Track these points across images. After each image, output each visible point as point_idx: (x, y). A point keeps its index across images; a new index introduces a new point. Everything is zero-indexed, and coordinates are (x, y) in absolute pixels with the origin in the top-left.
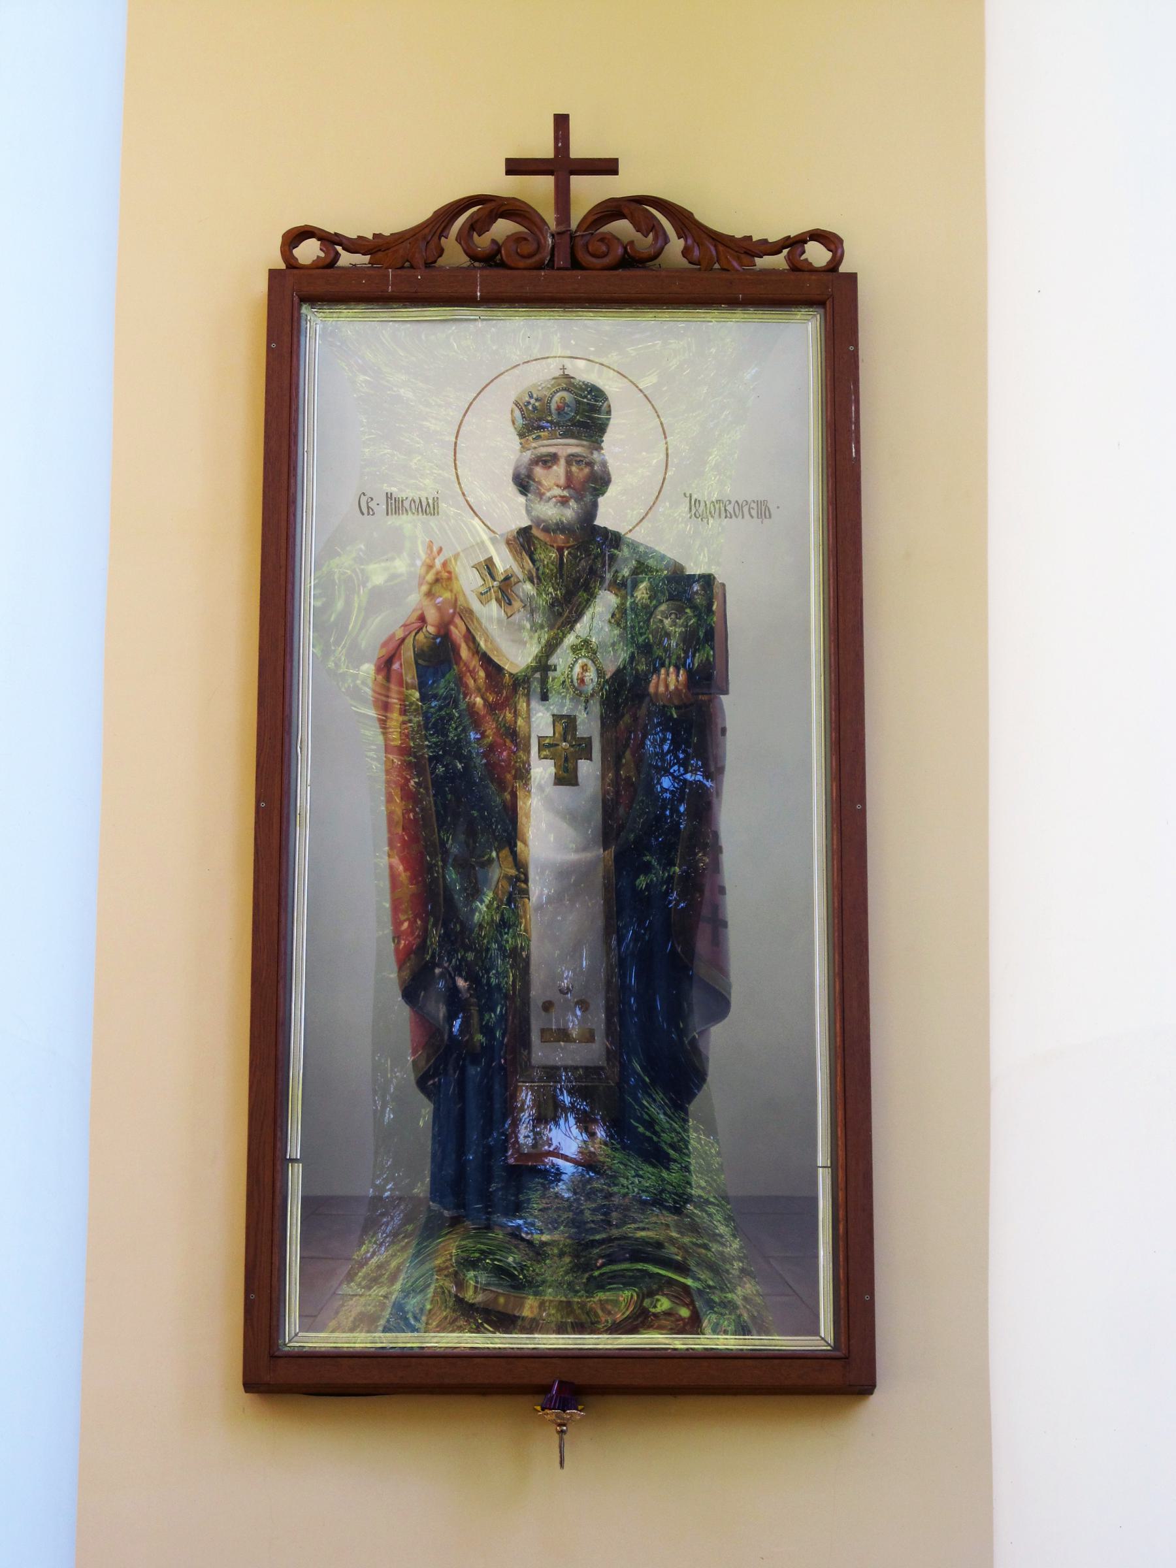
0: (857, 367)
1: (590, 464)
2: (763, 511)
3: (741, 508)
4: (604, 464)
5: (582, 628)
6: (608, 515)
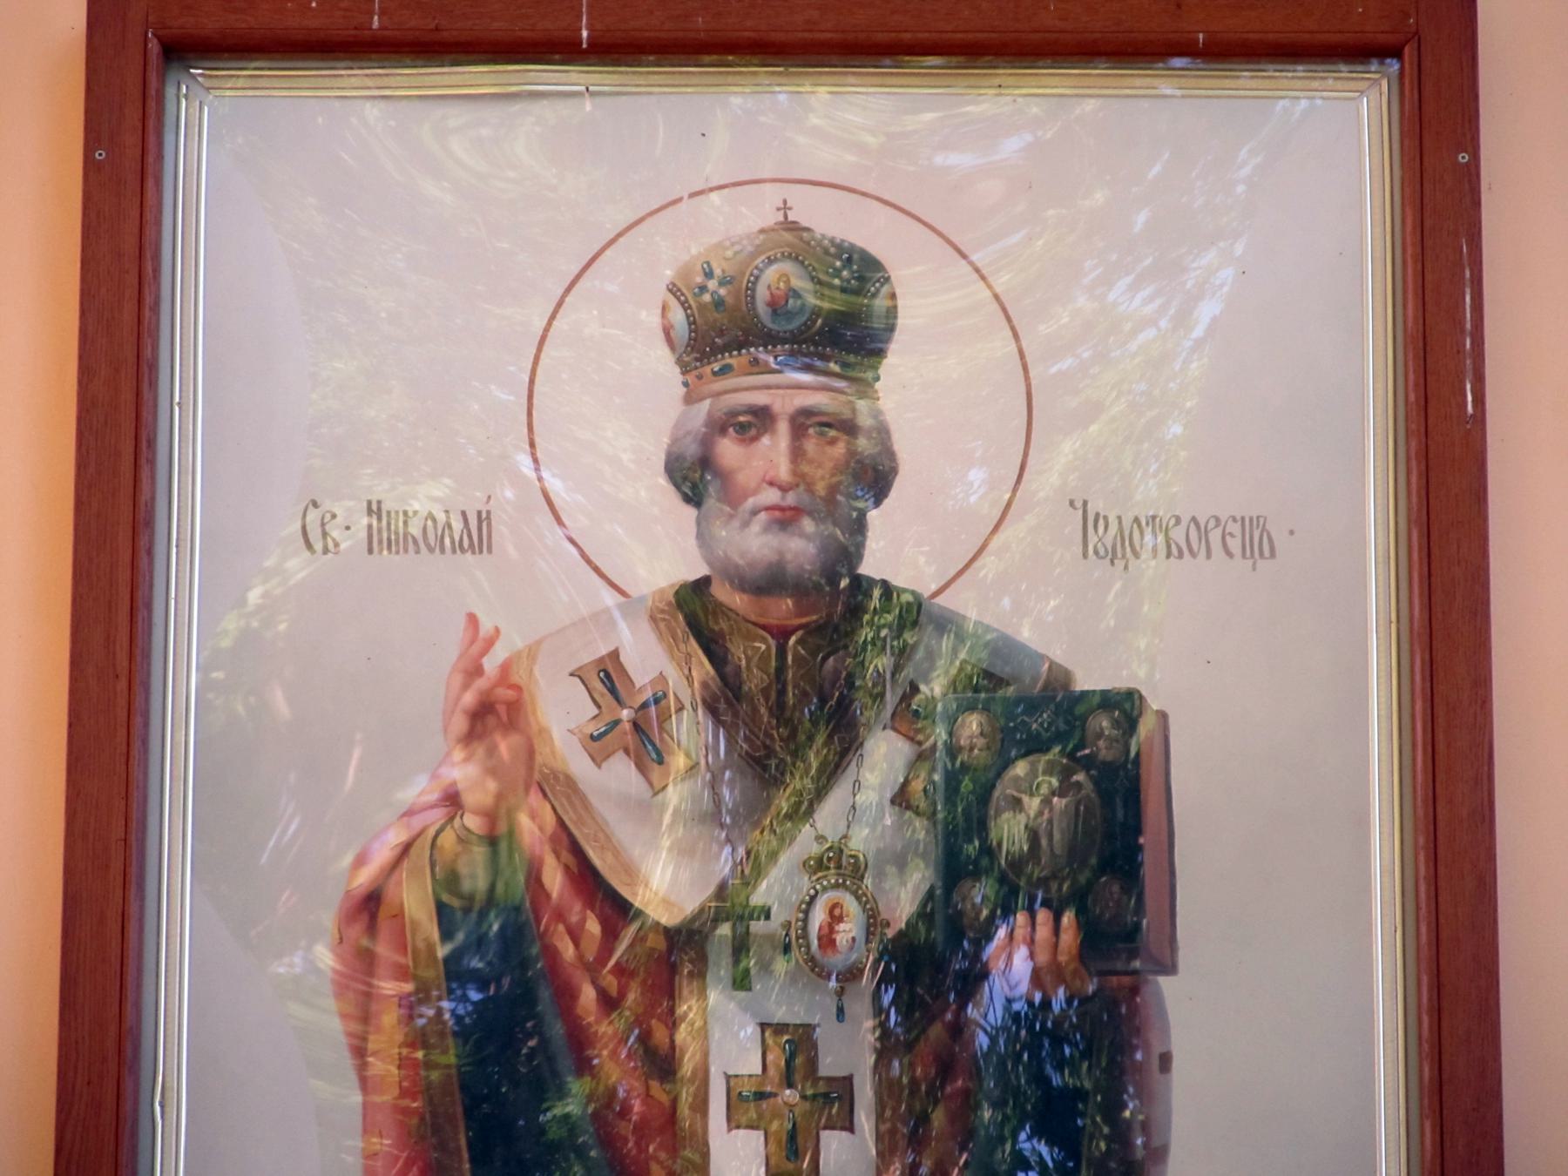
0: (1477, 203)
1: (849, 428)
2: (1255, 540)
3: (1204, 534)
4: (882, 433)
5: (828, 817)
6: (896, 550)
